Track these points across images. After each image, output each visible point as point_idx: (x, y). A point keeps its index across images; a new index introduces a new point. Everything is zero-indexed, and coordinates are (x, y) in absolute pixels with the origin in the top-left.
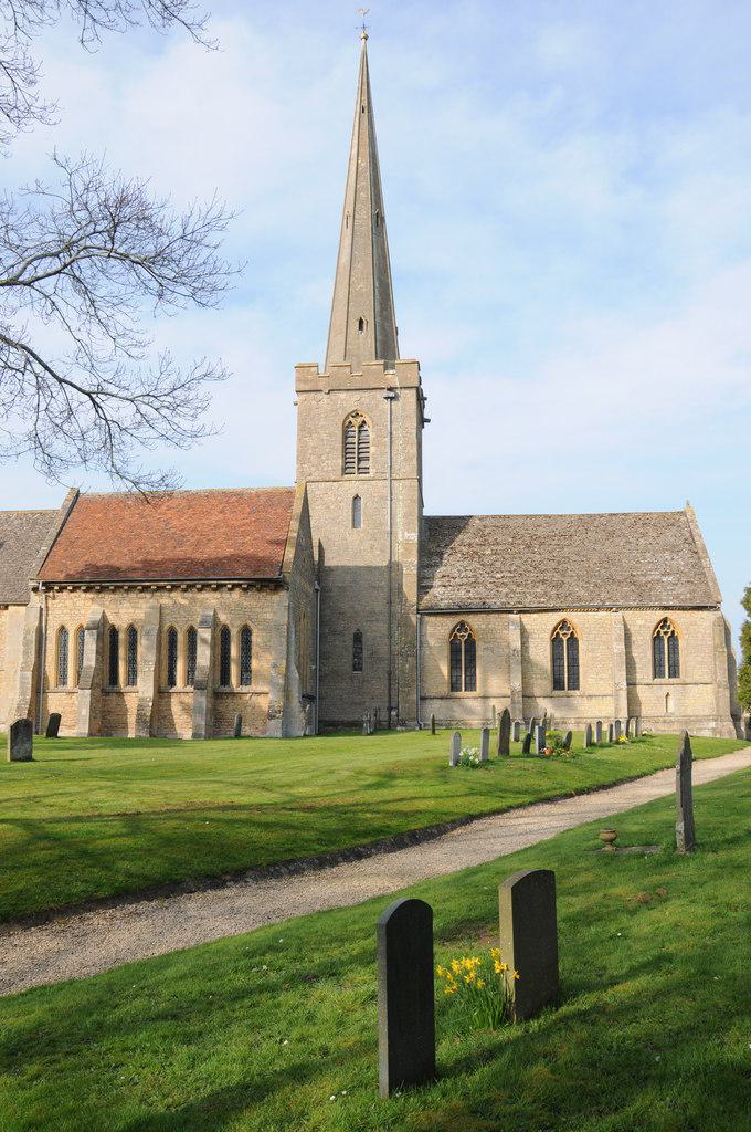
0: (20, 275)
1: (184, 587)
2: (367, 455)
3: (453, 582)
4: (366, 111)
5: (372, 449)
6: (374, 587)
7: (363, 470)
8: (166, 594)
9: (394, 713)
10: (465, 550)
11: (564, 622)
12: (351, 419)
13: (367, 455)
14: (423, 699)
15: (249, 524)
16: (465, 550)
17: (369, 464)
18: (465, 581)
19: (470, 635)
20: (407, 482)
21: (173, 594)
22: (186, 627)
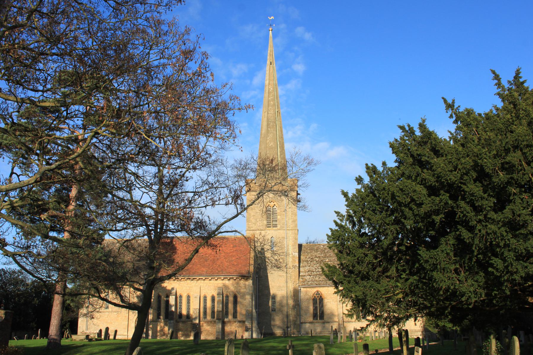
0: (238, 211)
1: (216, 278)
2: (276, 219)
3: (313, 273)
4: (272, 64)
5: (279, 217)
6: (280, 276)
7: (275, 226)
8: (203, 281)
9: (289, 329)
10: (317, 259)
11: (317, 291)
12: (269, 204)
13: (276, 219)
14: (302, 323)
15: (233, 252)
16: (317, 259)
17: (277, 223)
18: (318, 273)
19: (321, 296)
20: (293, 231)
21: (206, 281)
22: (211, 295)
